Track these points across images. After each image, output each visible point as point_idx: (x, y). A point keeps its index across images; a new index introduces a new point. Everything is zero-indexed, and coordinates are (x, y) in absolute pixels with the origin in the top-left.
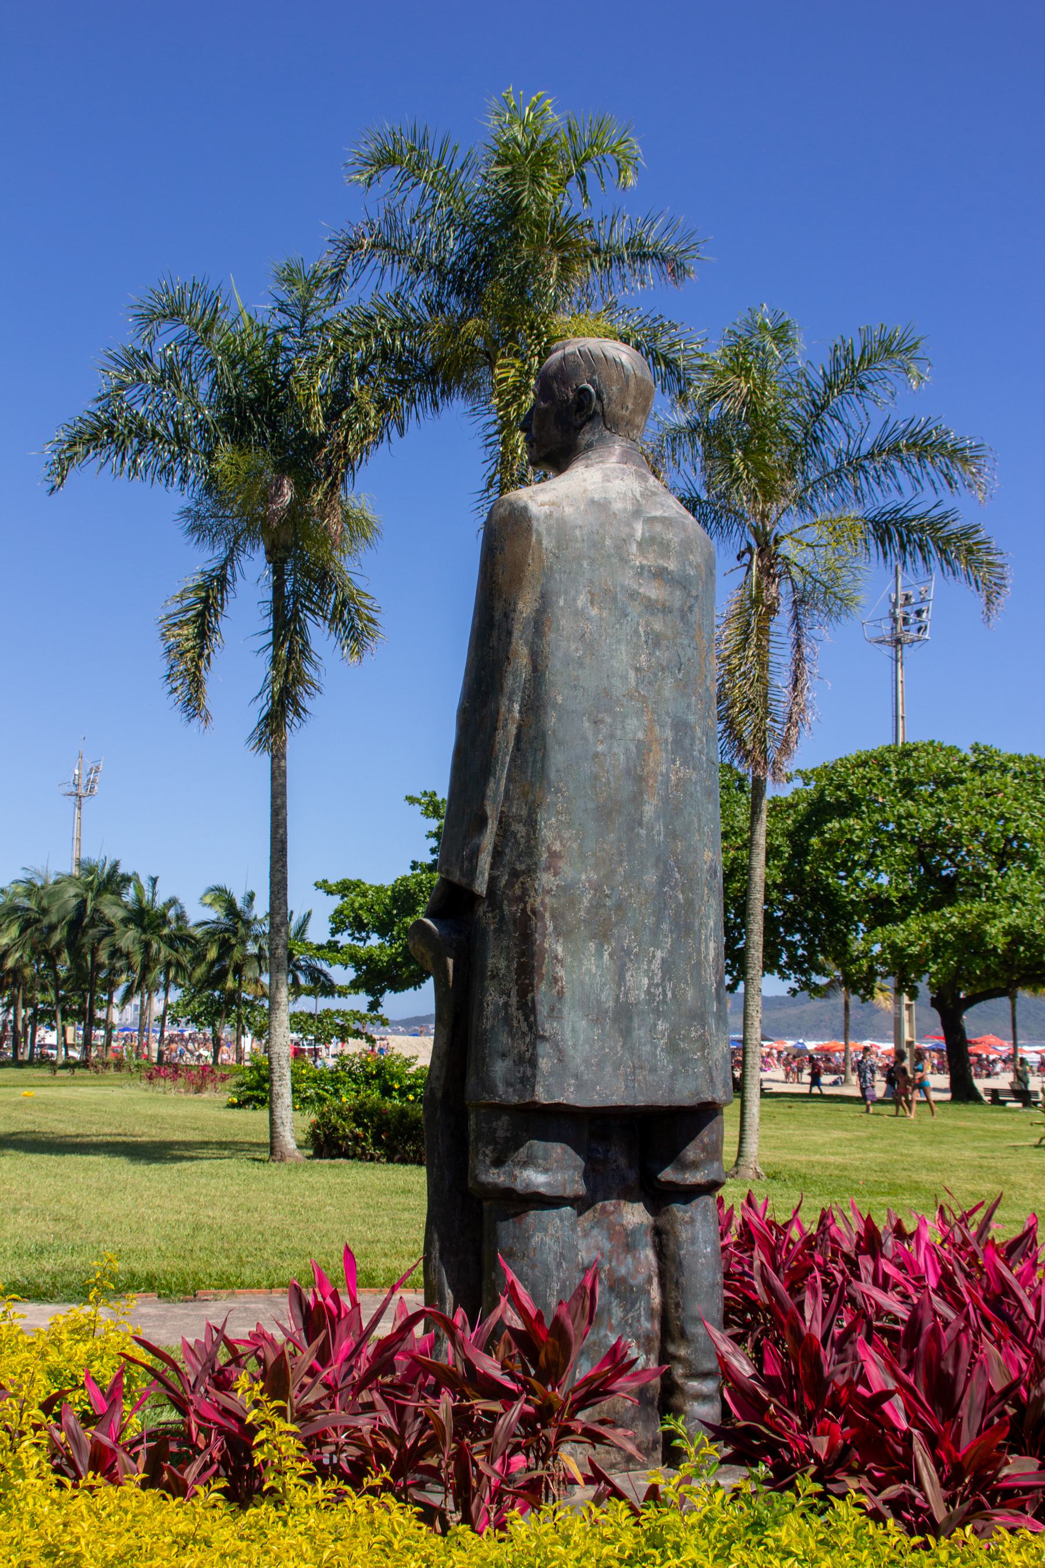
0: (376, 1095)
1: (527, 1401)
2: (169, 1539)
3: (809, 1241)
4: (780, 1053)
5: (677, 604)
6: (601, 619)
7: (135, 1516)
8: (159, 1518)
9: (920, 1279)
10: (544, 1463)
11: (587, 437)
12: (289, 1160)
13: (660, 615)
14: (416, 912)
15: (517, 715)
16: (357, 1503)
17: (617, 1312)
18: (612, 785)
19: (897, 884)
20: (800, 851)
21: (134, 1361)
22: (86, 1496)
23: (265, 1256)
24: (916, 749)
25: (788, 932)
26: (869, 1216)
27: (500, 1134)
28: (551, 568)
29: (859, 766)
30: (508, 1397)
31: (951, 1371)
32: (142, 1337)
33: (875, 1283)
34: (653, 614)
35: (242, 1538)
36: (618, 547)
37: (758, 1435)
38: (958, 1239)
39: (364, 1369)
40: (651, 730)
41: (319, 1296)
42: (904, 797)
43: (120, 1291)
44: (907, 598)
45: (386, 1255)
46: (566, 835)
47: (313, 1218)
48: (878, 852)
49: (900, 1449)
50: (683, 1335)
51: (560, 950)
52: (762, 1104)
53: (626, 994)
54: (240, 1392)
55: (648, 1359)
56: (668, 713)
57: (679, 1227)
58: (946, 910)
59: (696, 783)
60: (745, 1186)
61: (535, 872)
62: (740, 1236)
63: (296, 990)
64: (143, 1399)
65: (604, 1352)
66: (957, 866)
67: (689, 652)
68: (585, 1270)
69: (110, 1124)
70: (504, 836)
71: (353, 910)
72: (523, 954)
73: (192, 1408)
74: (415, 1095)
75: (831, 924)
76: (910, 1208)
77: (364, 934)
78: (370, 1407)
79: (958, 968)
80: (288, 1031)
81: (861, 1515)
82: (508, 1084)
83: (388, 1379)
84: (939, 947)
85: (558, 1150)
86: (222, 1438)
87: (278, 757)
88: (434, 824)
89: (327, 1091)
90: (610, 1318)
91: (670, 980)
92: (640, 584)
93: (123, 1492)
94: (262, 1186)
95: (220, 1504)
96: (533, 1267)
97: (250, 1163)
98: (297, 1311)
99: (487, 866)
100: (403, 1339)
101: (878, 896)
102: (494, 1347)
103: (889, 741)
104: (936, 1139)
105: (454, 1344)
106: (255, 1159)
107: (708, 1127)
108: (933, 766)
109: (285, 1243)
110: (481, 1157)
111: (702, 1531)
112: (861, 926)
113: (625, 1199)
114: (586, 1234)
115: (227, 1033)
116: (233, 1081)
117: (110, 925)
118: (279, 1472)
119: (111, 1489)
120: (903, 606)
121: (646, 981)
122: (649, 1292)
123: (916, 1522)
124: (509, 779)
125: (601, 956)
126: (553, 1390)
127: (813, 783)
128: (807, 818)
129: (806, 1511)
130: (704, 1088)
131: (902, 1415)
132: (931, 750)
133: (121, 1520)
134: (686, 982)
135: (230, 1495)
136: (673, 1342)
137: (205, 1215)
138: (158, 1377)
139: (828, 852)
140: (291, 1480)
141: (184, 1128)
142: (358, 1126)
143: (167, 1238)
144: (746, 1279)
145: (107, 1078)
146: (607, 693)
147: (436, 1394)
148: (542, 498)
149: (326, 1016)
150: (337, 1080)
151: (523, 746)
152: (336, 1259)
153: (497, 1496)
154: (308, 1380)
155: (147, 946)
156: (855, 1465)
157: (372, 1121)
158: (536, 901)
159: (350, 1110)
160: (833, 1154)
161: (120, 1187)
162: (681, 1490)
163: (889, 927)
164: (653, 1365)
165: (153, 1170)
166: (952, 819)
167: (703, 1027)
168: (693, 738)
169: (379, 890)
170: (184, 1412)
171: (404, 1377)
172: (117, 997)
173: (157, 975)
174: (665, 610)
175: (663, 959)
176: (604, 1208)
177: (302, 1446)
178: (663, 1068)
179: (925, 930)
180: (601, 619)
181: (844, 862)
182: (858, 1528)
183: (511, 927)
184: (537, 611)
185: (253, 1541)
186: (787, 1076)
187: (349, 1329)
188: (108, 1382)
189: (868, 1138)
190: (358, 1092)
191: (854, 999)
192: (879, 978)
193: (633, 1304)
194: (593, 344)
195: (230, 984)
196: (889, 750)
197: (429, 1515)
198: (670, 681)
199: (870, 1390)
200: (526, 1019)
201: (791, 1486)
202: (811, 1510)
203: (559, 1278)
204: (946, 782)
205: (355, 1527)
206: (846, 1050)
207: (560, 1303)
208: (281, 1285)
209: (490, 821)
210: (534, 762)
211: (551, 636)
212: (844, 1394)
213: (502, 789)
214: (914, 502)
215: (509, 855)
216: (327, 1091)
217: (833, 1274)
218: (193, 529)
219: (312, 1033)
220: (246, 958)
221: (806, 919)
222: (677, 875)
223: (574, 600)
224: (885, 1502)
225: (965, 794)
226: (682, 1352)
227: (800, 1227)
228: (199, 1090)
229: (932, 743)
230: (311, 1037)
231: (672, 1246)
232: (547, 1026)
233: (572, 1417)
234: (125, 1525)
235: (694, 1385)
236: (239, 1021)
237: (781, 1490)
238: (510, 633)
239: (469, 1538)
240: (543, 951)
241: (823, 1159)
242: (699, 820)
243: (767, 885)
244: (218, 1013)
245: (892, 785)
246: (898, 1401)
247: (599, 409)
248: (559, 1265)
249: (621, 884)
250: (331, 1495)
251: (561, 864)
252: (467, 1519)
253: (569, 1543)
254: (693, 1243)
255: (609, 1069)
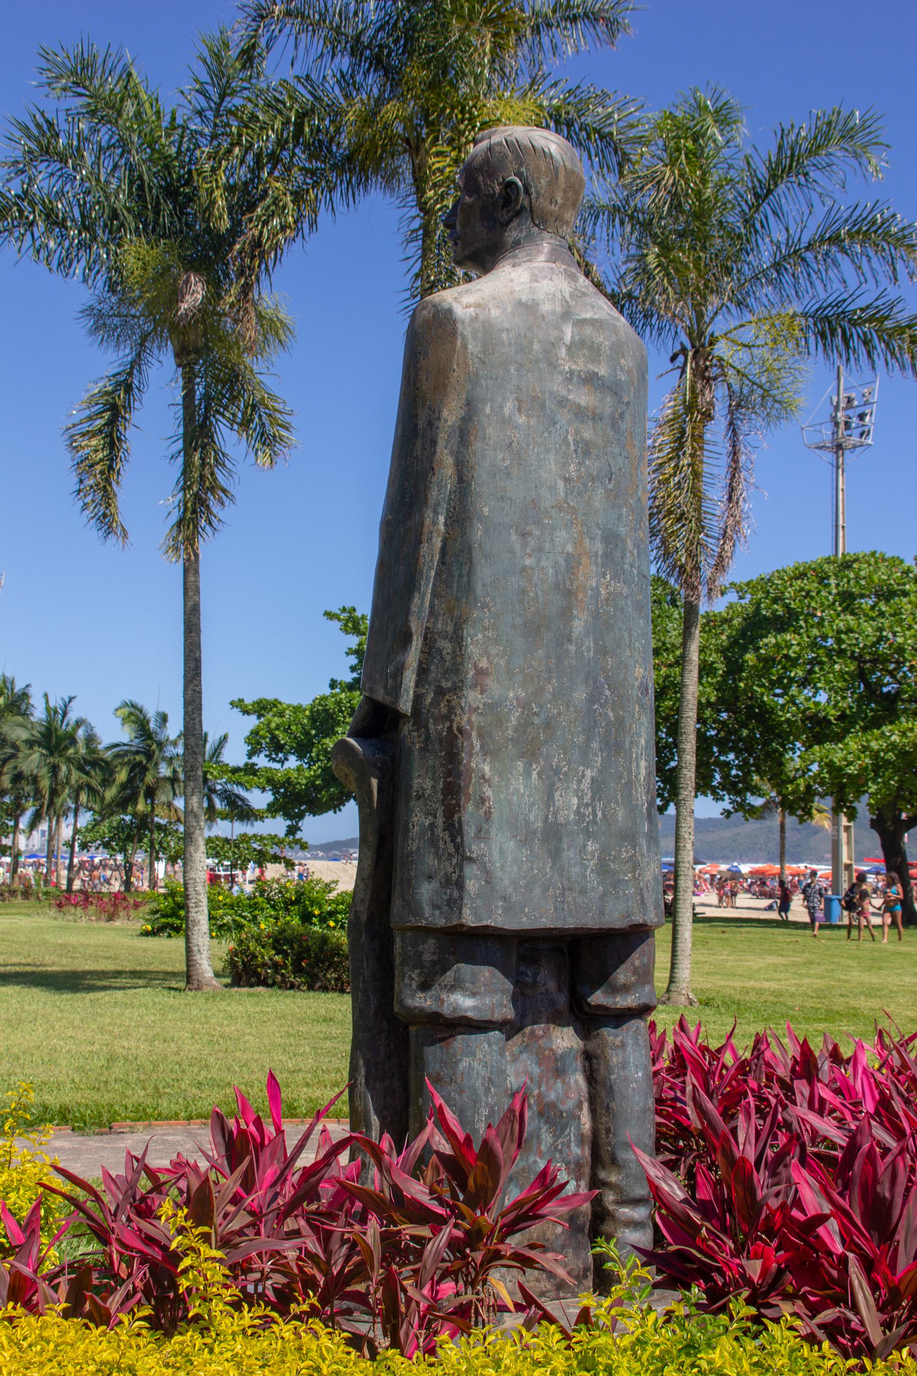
0: (296, 921)
1: (456, 1226)
2: (92, 1368)
3: (743, 1067)
4: (713, 876)
5: (608, 411)
6: (529, 427)
7: (57, 1346)
8: (82, 1347)
9: (858, 1104)
10: (473, 1288)
11: (514, 234)
12: (206, 989)
13: (590, 423)
14: (335, 733)
15: (442, 528)
16: (285, 1329)
17: (547, 1138)
18: (541, 600)
19: (837, 702)
20: (735, 668)
21: (53, 1191)
22: (5, 1326)
23: (183, 1087)
24: (856, 560)
25: (722, 752)
26: (805, 1041)
27: (427, 957)
28: (477, 374)
29: (797, 578)
30: (436, 1222)
31: (887, 1195)
32: (60, 1165)
33: (811, 1107)
34: (582, 422)
35: (167, 1365)
36: (546, 352)
37: (692, 1259)
38: (896, 1062)
39: (288, 1196)
40: (581, 543)
41: (242, 1121)
42: (844, 610)
43: (30, 1125)
44: (850, 400)
45: (307, 1085)
46: (493, 651)
47: (232, 1048)
48: (817, 669)
49: (835, 1273)
50: (614, 1160)
51: (487, 769)
52: (694, 930)
53: (555, 814)
54: (163, 1219)
55: (578, 1186)
56: (598, 525)
57: (609, 1052)
58: (886, 729)
59: (626, 597)
60: (677, 1013)
61: (461, 689)
62: (673, 1061)
63: (211, 813)
64: (62, 1231)
65: (533, 1177)
66: (900, 683)
67: (620, 461)
68: (514, 1095)
69: (18, 954)
70: (429, 653)
71: (270, 731)
72: (449, 773)
73: (113, 1237)
74: (336, 922)
75: (767, 743)
76: (849, 1035)
77: (281, 755)
78: (296, 1233)
79: (900, 788)
80: (204, 856)
81: (796, 1337)
82: (435, 907)
83: (314, 1207)
84: (879, 766)
85: (486, 973)
86: (146, 1268)
87: (191, 569)
88: (353, 641)
89: (244, 917)
90: (540, 1144)
91: (600, 800)
92: (569, 391)
93: (45, 1322)
94: (178, 1015)
95: (144, 1332)
96: (461, 1092)
97: (165, 992)
98: (219, 1139)
99: (412, 684)
100: (329, 1165)
101: (816, 715)
102: (422, 1172)
103: (828, 552)
104: (875, 964)
105: (380, 1170)
106: (170, 988)
107: (639, 950)
108: (875, 578)
109: (203, 1073)
110: (407, 981)
111: (634, 1353)
112: (798, 745)
113: (554, 1023)
114: (515, 1059)
115: (140, 858)
116: (147, 908)
117: (14, 746)
118: (204, 1299)
119: (32, 1319)
120: (845, 409)
121: (575, 801)
122: (579, 1119)
123: (853, 1346)
124: (435, 594)
125: (530, 776)
126: (482, 1214)
127: (748, 596)
128: (743, 633)
129: (740, 1334)
130: (635, 910)
131: (837, 1239)
132: (872, 561)
133: (43, 1350)
134: (617, 802)
135: (154, 1323)
136: (604, 1167)
137: (121, 1046)
138: (80, 1207)
139: (763, 668)
140: (217, 1306)
141: (96, 958)
142: (277, 954)
143: (80, 1069)
144: (679, 1105)
145: (14, 906)
146: (535, 504)
147: (363, 1221)
148: (467, 299)
149: (242, 842)
150: (254, 906)
151: (448, 559)
152: (256, 1089)
153: (426, 1323)
154: (231, 1208)
155: (55, 769)
156: (790, 1289)
157: (292, 948)
158: (463, 720)
159: (269, 937)
160: (768, 980)
161: (31, 1019)
162: (613, 1312)
163: (827, 746)
164: (583, 1190)
165: (65, 1000)
166: (895, 634)
167: (634, 847)
168: (624, 551)
169: (297, 709)
170: (106, 1241)
171: (330, 1204)
172: (23, 824)
173: (65, 798)
174: (596, 417)
175: (592, 778)
176: (532, 1032)
177: (227, 1272)
178: (593, 889)
179: (865, 749)
180: (529, 427)
181: (780, 679)
182: (792, 1351)
183: (437, 747)
184: (463, 419)
185: (178, 1368)
186: (720, 900)
187: (273, 1156)
188: (24, 1214)
189: (804, 964)
190: (277, 919)
191: (791, 821)
192: (817, 798)
193: (563, 1130)
194: (522, 133)
195: (141, 806)
196: (828, 561)
197: (356, 1341)
198: (600, 491)
199: (803, 1211)
200: (453, 840)
201: (724, 1309)
202: (745, 1333)
203: (487, 1104)
204: (887, 594)
205: (283, 1353)
206: (781, 874)
207: (489, 1126)
208: (200, 1116)
209: (415, 638)
210: (460, 576)
211: (477, 445)
212: (778, 1217)
213: (427, 604)
214: (857, 293)
215: (434, 672)
216: (244, 917)
217: (767, 1100)
218: (96, 329)
219: (228, 858)
220: (158, 780)
221: (740, 739)
222: (607, 692)
223: (501, 407)
224: (820, 1326)
225: (909, 606)
226: (613, 1178)
227: (734, 1052)
228: (111, 918)
229: (873, 554)
230: (227, 863)
231: (602, 1071)
232: (474, 847)
233: (502, 1241)
234: (46, 1356)
235: (626, 1212)
236: (152, 846)
237: (716, 1313)
238: (434, 442)
239: (399, 1362)
240: (470, 770)
241: (757, 985)
242: (630, 636)
243: (700, 703)
244: (130, 838)
245: (831, 598)
246: (833, 1224)
247: (526, 204)
248: (488, 1090)
249: (550, 702)
250: (257, 1322)
251: (488, 681)
252: (395, 1343)
253: (499, 1367)
254: (624, 1068)
255: (537, 891)
